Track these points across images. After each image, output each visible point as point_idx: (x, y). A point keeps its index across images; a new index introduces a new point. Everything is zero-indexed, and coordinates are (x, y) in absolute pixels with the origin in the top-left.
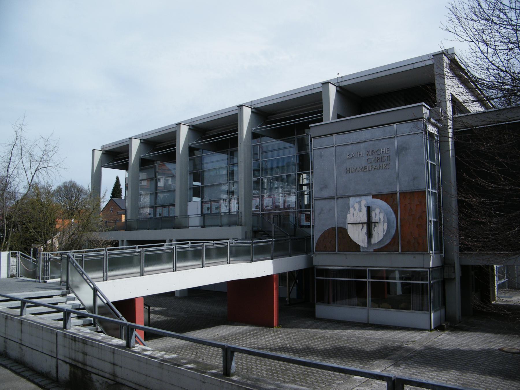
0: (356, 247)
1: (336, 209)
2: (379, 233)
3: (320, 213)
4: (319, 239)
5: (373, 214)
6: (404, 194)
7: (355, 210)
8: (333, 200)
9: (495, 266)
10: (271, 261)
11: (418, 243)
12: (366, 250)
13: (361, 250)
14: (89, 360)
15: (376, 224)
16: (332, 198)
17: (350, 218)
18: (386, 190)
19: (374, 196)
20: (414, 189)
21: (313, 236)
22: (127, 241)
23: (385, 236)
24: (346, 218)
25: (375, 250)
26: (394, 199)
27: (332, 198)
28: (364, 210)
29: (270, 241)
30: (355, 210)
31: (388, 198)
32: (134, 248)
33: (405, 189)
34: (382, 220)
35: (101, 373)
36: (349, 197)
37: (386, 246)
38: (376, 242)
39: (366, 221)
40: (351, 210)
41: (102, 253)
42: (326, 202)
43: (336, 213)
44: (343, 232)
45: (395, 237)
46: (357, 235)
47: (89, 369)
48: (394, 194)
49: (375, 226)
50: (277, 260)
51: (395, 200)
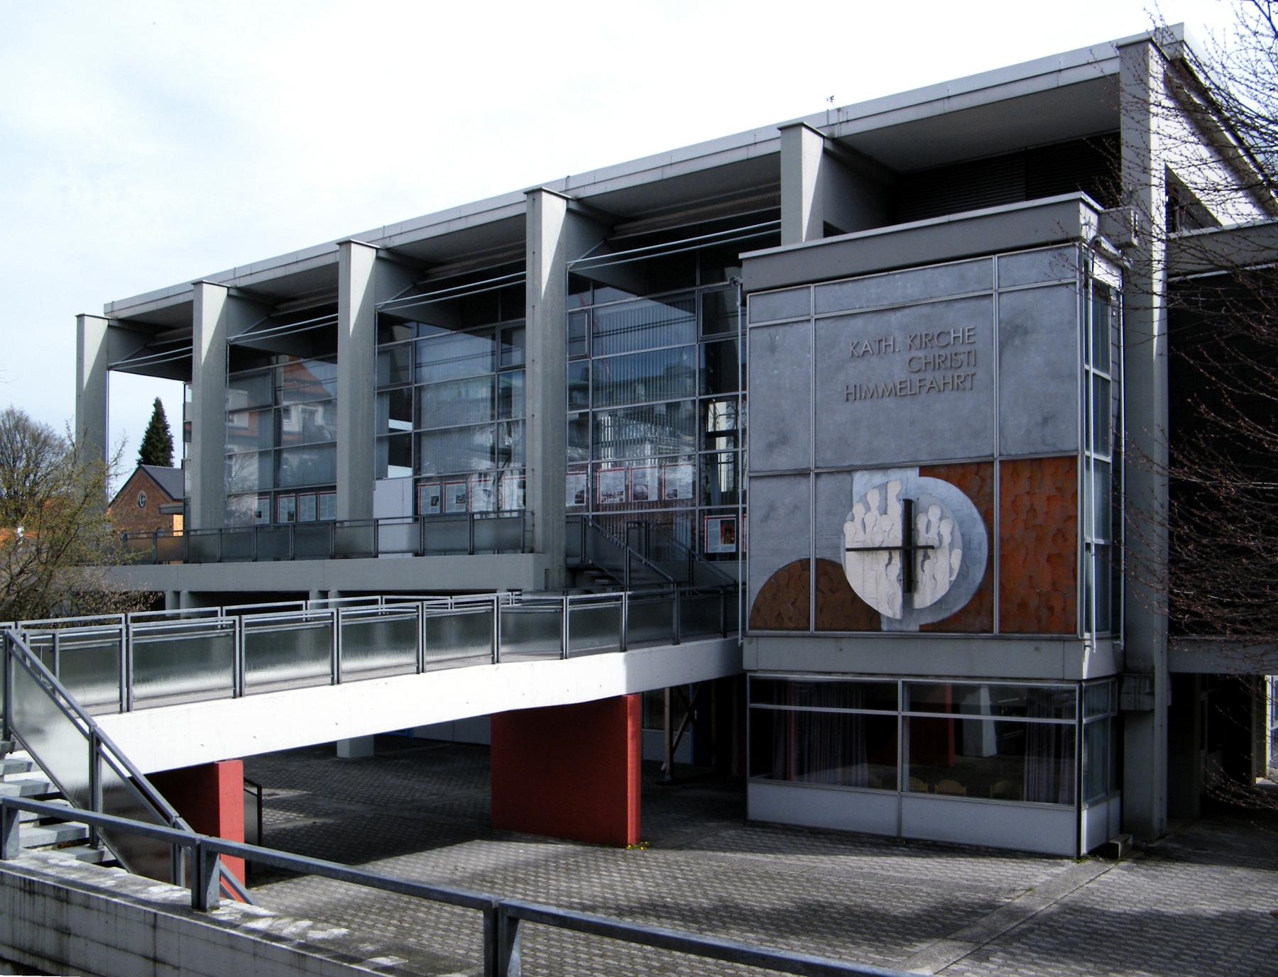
0: (868, 618)
1: (812, 507)
2: (938, 577)
3: (766, 518)
4: (762, 592)
5: (921, 523)
6: (1012, 466)
7: (868, 509)
11: (1051, 609)
13: (884, 627)
15: (930, 552)
16: (803, 474)
17: (853, 534)
18: (960, 452)
19: (926, 471)
20: (1042, 449)
21: (744, 584)
23: (954, 586)
24: (840, 533)
25: (924, 628)
26: (983, 480)
27: (803, 474)
28: (896, 510)
30: (868, 509)
31: (966, 475)
32: (214, 614)
33: (1017, 450)
34: (947, 539)
36: (850, 471)
38: (929, 604)
39: (899, 543)
40: (858, 509)
41: (115, 628)
42: (783, 484)
44: (832, 572)
45: (983, 592)
46: (874, 583)
48: (983, 466)
49: (926, 557)
51: (986, 481)
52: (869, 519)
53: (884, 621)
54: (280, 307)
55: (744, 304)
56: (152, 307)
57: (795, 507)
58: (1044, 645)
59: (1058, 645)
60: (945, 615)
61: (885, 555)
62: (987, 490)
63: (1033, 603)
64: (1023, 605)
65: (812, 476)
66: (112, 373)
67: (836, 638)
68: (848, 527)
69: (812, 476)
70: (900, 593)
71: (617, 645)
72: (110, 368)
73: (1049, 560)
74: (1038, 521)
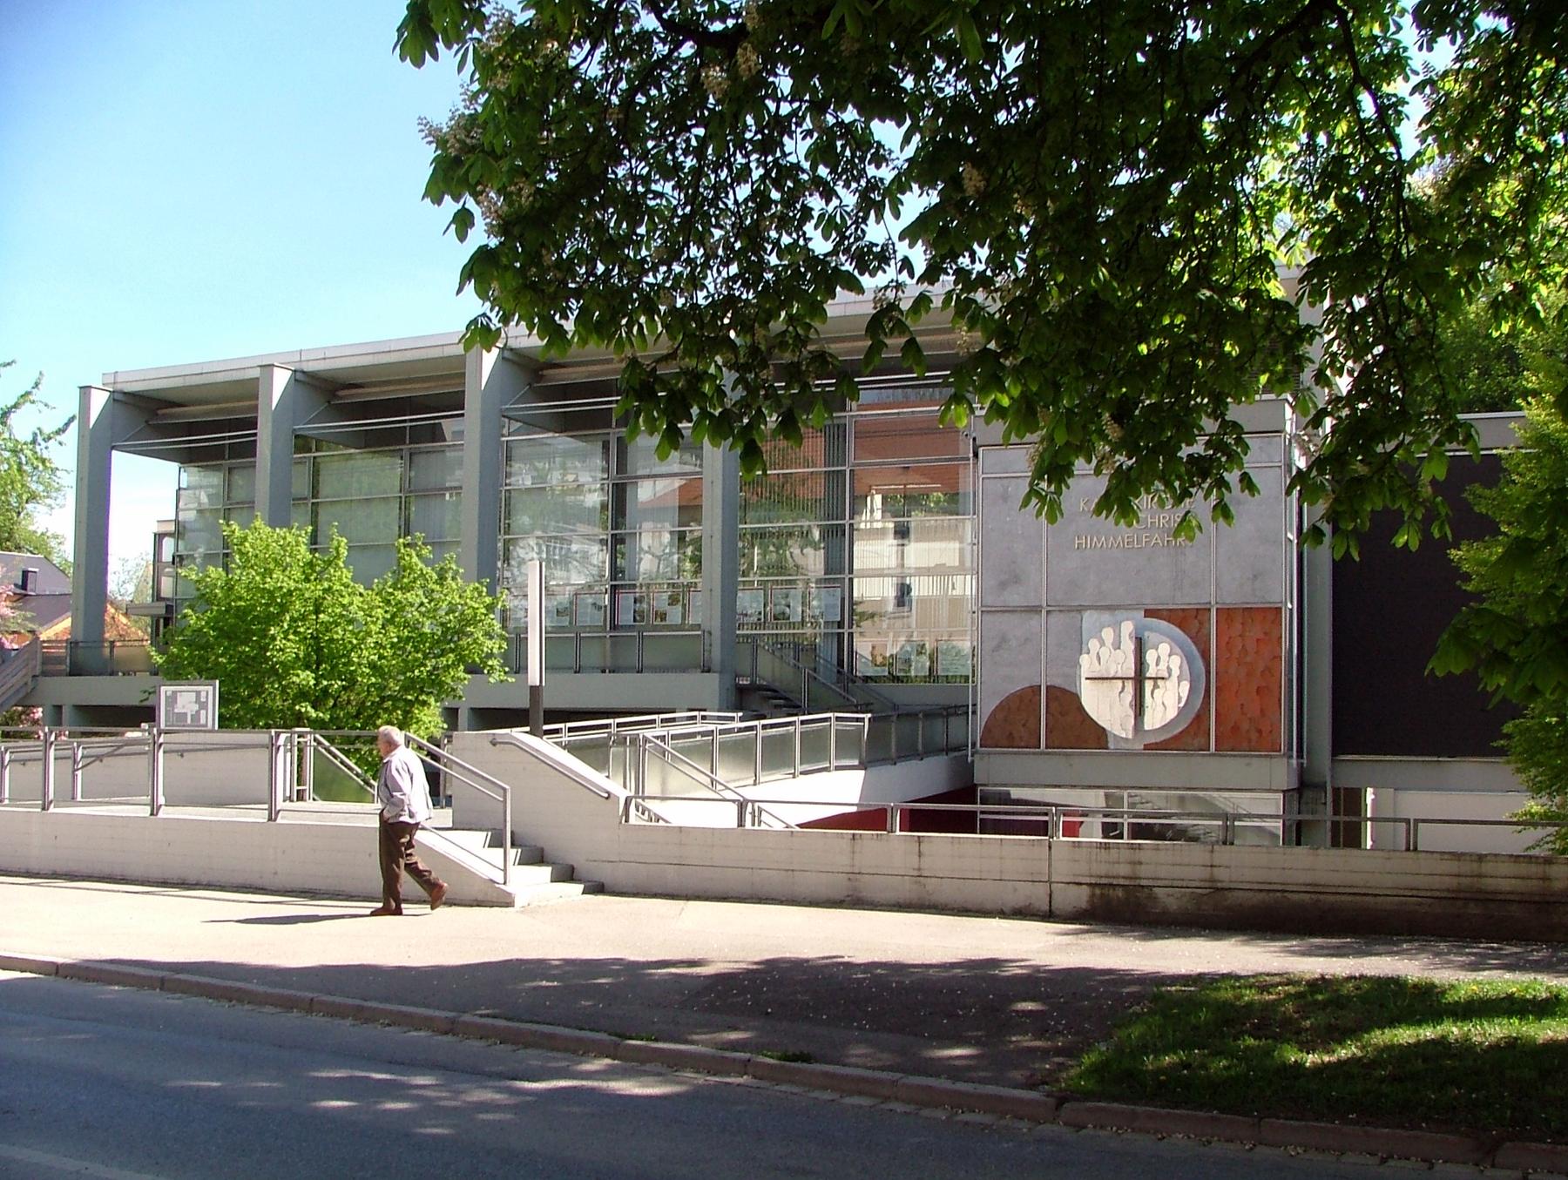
0: (1094, 736)
1: (1043, 639)
2: (1167, 704)
3: (998, 648)
4: (994, 713)
5: (1150, 656)
6: (1226, 614)
7: (1102, 644)
8: (1037, 617)
9: (1370, 795)
10: (862, 773)
11: (1260, 732)
12: (1129, 746)
13: (1111, 745)
14: (1143, 871)
15: (1160, 682)
16: (1035, 610)
17: (1087, 665)
18: (1186, 599)
19: (1149, 613)
20: (1254, 601)
21: (974, 705)
22: (79, 708)
23: (1181, 711)
24: (1077, 665)
25: (1147, 747)
26: (1201, 623)
27: (1035, 610)
28: (1129, 646)
29: (862, 720)
30: (1102, 644)
31: (1187, 620)
32: (732, 719)
33: (1232, 599)
34: (1176, 672)
35: (1176, 883)
36: (1081, 609)
37: (1176, 738)
38: (1158, 726)
39: (1132, 674)
40: (1093, 644)
41: (791, 728)
42: (1014, 619)
43: (1043, 646)
44: (1066, 701)
45: (1200, 719)
46: (1105, 706)
47: (1143, 882)
48: (1201, 613)
49: (1156, 686)
50: (873, 770)
51: (1203, 624)
52: (1104, 652)
53: (1110, 739)
54: (341, 393)
55: (976, 455)
56: (179, 383)
57: (1027, 640)
58: (1255, 760)
59: (1265, 762)
60: (1169, 736)
61: (1120, 683)
62: (1204, 631)
63: (1245, 726)
64: (1236, 729)
65: (1044, 613)
66: (118, 457)
67: (1066, 754)
68: (1084, 660)
69: (1044, 613)
70: (1132, 714)
71: (856, 762)
72: (113, 448)
73: (1258, 691)
74: (1248, 659)
